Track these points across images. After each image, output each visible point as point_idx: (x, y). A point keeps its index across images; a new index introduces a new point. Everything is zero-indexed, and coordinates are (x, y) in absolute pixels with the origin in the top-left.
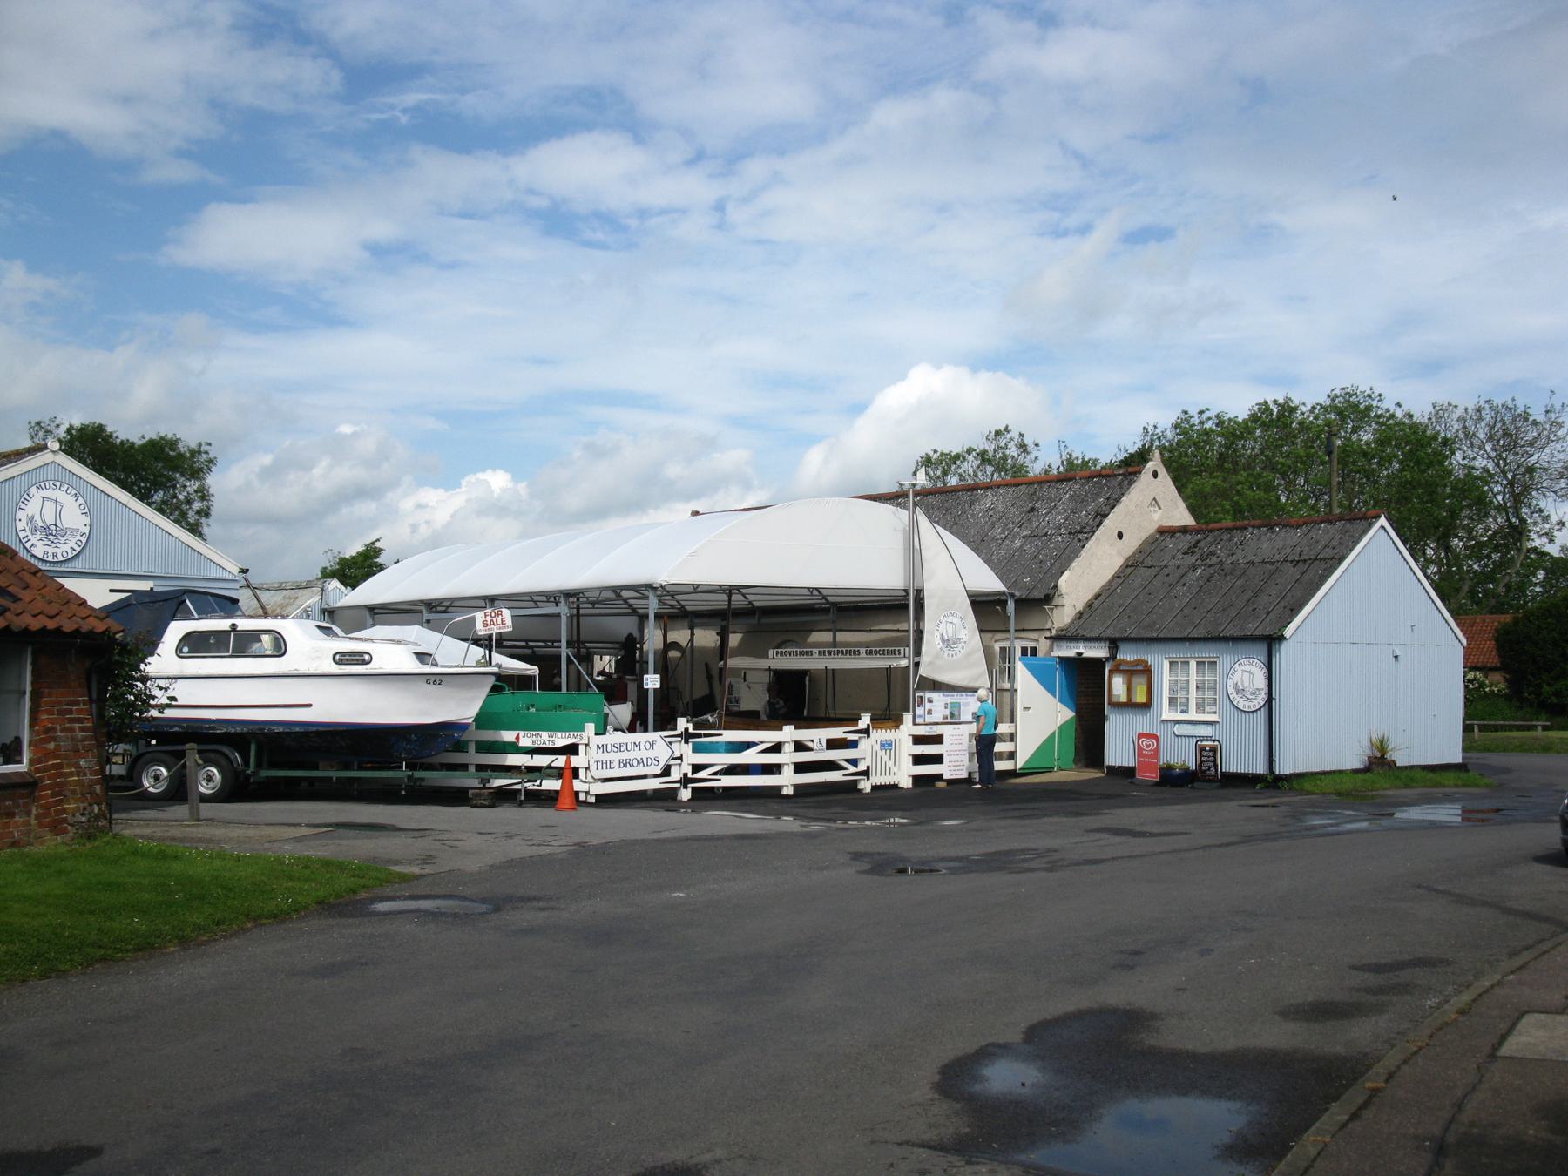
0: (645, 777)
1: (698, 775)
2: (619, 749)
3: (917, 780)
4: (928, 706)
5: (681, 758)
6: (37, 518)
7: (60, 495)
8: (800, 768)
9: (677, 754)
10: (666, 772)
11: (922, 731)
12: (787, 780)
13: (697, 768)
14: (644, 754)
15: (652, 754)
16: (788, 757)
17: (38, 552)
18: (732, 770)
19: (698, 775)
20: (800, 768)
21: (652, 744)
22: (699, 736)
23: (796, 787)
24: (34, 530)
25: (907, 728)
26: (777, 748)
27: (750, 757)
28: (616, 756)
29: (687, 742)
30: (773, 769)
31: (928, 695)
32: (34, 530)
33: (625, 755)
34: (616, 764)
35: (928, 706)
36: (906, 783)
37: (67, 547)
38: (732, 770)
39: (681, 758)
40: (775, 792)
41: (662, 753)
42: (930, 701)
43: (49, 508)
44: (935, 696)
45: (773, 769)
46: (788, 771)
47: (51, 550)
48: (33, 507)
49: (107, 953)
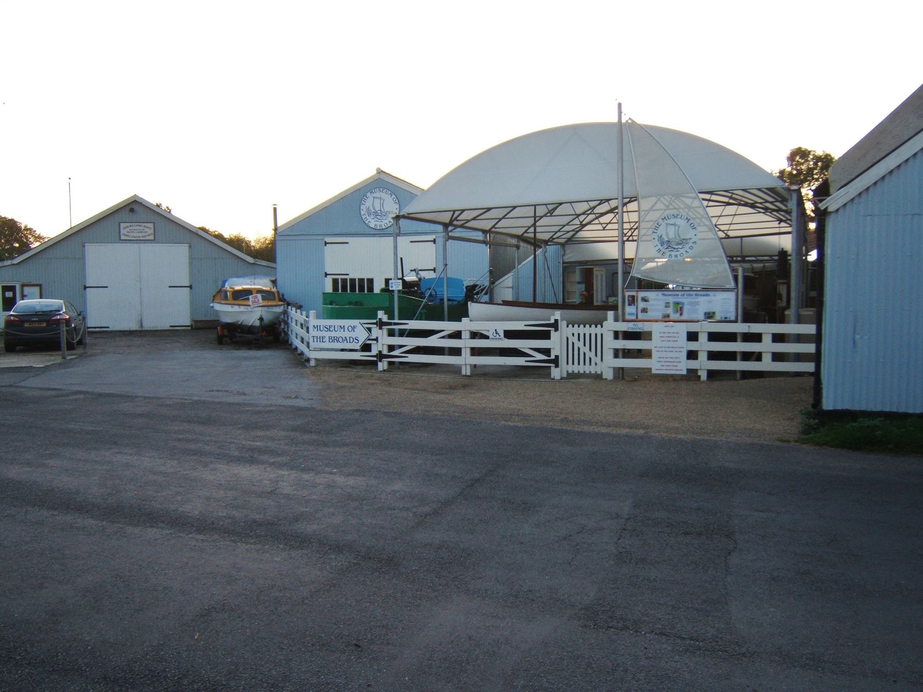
0: (342, 350)
1: (392, 353)
2: (329, 330)
3: (620, 373)
4: (641, 305)
5: (376, 340)
6: (371, 208)
7: (383, 195)
8: (475, 352)
9: (374, 337)
10: (366, 348)
11: (623, 327)
12: (466, 361)
13: (391, 348)
14: (347, 334)
15: (353, 335)
16: (466, 343)
17: (372, 225)
18: (418, 350)
19: (392, 353)
20: (475, 352)
21: (354, 328)
22: (390, 324)
23: (688, 370)
24: (369, 214)
25: (611, 324)
26: (457, 335)
27: (432, 341)
28: (327, 334)
29: (380, 328)
30: (456, 352)
31: (642, 294)
32: (369, 214)
33: (333, 334)
34: (327, 339)
35: (641, 305)
36: (609, 375)
37: (387, 221)
38: (418, 350)
39: (376, 340)
40: (456, 370)
41: (362, 336)
42: (645, 300)
43: (377, 202)
44: (651, 295)
45: (456, 352)
46: (466, 353)
47: (378, 223)
48: (368, 203)
49: (207, 421)
